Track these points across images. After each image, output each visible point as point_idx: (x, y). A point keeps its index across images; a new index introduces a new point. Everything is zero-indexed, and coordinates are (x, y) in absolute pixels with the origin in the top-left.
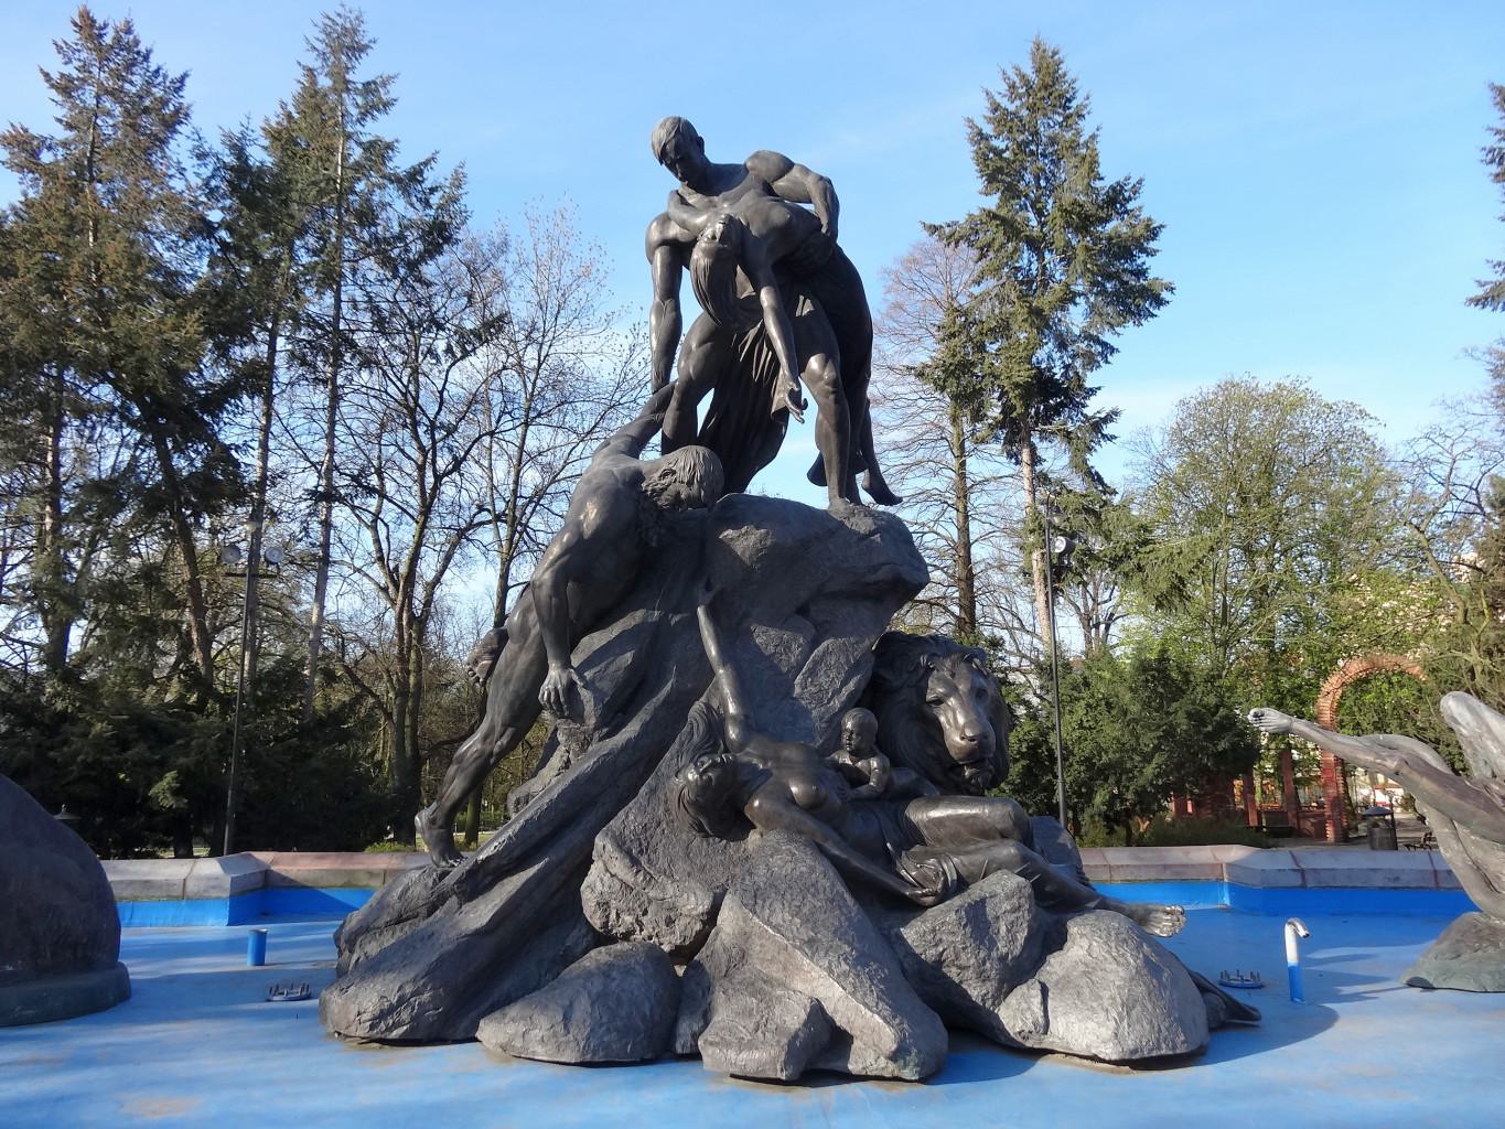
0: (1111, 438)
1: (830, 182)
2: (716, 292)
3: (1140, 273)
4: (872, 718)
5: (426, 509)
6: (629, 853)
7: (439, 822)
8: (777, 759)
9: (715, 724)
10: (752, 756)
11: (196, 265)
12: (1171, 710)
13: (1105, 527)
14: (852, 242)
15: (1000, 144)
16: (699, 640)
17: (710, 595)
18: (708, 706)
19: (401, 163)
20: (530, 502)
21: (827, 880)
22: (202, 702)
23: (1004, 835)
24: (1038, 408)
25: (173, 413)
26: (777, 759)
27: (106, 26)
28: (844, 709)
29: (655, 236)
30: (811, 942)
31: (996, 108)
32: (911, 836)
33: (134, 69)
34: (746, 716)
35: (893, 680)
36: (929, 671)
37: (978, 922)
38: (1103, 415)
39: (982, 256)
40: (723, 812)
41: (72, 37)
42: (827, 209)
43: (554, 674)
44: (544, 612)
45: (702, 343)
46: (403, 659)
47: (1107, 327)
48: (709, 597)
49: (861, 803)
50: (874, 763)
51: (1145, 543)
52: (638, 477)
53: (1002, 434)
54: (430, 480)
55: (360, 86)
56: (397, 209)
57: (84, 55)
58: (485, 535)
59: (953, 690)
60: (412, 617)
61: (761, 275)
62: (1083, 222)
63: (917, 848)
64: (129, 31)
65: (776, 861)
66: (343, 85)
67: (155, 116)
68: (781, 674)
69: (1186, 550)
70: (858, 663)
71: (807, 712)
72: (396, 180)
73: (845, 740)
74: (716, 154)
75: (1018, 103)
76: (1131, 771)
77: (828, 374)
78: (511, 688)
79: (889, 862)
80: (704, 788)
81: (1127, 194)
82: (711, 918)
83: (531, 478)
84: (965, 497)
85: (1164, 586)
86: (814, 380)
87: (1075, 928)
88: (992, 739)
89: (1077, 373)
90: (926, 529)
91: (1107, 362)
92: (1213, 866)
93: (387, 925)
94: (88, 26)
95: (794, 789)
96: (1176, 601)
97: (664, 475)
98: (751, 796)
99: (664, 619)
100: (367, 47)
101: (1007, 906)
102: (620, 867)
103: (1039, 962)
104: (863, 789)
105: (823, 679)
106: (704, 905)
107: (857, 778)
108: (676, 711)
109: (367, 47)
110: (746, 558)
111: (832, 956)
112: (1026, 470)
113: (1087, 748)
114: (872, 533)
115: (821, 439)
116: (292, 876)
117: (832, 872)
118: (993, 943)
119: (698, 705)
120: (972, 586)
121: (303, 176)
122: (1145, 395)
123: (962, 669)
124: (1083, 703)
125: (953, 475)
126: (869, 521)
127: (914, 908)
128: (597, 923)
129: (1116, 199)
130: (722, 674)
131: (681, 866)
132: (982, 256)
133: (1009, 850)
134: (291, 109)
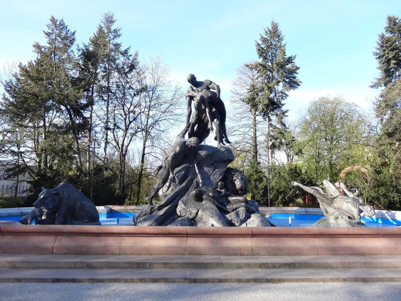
0: (287, 116)
1: (219, 86)
2: (198, 108)
3: (295, 78)
4: (223, 183)
5: (127, 129)
6: (184, 204)
7: (150, 199)
8: (208, 189)
9: (198, 184)
10: (203, 189)
11: (75, 73)
12: (297, 179)
13: (285, 137)
14: (223, 97)
15: (263, 46)
16: (195, 169)
17: (197, 162)
18: (196, 181)
19: (122, 49)
20: (151, 126)
21: (215, 208)
22: (80, 174)
23: (243, 202)
24: (271, 108)
25: (76, 110)
26: (208, 189)
27: (57, 20)
28: (219, 181)
29: (187, 95)
30: (212, 216)
31: (262, 37)
32: (229, 202)
33: (63, 30)
34: (203, 182)
35: (228, 176)
36: (234, 175)
37: (237, 214)
38: (285, 111)
39: (258, 72)
40: (199, 198)
41: (50, 23)
42: (218, 92)
43: (171, 175)
44: (170, 165)
45: (195, 116)
46: (121, 164)
47: (286, 90)
48: (197, 162)
49: (220, 197)
50: (223, 190)
51: (294, 141)
52: (185, 142)
53: (262, 114)
54: (128, 122)
55: (113, 31)
56: (121, 60)
57: (52, 27)
58: (139, 134)
59: (238, 178)
60: (123, 154)
61: (206, 106)
62: (281, 66)
63: (230, 204)
64: (62, 21)
65: (207, 205)
66: (109, 31)
67: (69, 40)
68: (208, 175)
69: (302, 143)
70: (222, 173)
71: (212, 182)
72: (121, 53)
73: (219, 187)
74: (198, 79)
75: (268, 36)
76: (287, 192)
77: (218, 123)
78: (163, 177)
79: (225, 206)
80: (196, 194)
81: (292, 58)
82: (197, 214)
83: (151, 121)
84: (255, 126)
85: (297, 151)
86: (215, 123)
87: (252, 215)
88: (244, 186)
89: (280, 101)
90: (246, 133)
91: (286, 98)
92: (291, 211)
93: (143, 216)
94: (53, 20)
95: (210, 194)
96: (300, 154)
97: (189, 142)
98: (203, 195)
99: (189, 166)
100: (114, 21)
101: (242, 212)
102: (183, 206)
103: (247, 220)
104: (221, 194)
105: (215, 176)
106: (196, 212)
107: (221, 193)
108: (191, 181)
109: (114, 21)
110: (203, 156)
111: (215, 218)
112: (267, 123)
113: (277, 187)
114: (225, 151)
115: (216, 133)
116: (116, 210)
117: (216, 207)
118: (239, 217)
119: (195, 180)
120: (257, 148)
121: (101, 52)
122: (297, 105)
123: (240, 175)
124: (277, 177)
125: (253, 120)
126: (224, 149)
127: (229, 213)
128: (179, 214)
129: (290, 60)
130: (199, 176)
131: (192, 206)
132: (258, 72)
133: (243, 204)
134: (96, 35)
